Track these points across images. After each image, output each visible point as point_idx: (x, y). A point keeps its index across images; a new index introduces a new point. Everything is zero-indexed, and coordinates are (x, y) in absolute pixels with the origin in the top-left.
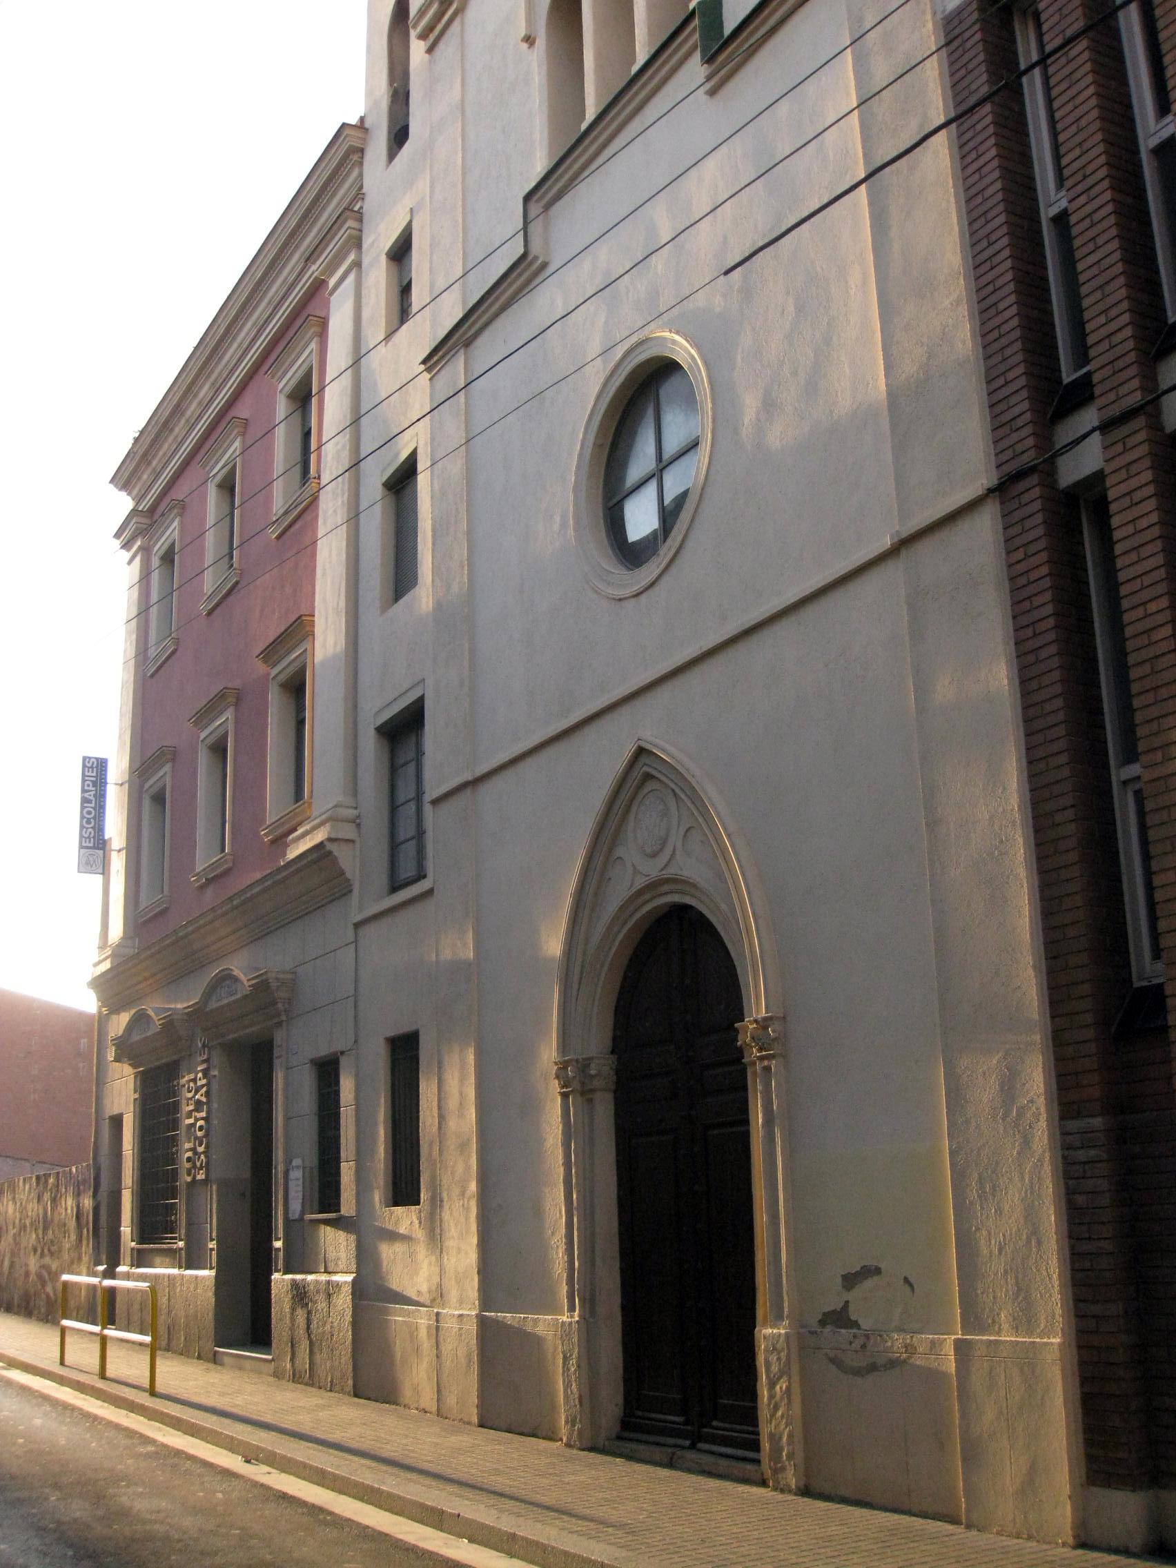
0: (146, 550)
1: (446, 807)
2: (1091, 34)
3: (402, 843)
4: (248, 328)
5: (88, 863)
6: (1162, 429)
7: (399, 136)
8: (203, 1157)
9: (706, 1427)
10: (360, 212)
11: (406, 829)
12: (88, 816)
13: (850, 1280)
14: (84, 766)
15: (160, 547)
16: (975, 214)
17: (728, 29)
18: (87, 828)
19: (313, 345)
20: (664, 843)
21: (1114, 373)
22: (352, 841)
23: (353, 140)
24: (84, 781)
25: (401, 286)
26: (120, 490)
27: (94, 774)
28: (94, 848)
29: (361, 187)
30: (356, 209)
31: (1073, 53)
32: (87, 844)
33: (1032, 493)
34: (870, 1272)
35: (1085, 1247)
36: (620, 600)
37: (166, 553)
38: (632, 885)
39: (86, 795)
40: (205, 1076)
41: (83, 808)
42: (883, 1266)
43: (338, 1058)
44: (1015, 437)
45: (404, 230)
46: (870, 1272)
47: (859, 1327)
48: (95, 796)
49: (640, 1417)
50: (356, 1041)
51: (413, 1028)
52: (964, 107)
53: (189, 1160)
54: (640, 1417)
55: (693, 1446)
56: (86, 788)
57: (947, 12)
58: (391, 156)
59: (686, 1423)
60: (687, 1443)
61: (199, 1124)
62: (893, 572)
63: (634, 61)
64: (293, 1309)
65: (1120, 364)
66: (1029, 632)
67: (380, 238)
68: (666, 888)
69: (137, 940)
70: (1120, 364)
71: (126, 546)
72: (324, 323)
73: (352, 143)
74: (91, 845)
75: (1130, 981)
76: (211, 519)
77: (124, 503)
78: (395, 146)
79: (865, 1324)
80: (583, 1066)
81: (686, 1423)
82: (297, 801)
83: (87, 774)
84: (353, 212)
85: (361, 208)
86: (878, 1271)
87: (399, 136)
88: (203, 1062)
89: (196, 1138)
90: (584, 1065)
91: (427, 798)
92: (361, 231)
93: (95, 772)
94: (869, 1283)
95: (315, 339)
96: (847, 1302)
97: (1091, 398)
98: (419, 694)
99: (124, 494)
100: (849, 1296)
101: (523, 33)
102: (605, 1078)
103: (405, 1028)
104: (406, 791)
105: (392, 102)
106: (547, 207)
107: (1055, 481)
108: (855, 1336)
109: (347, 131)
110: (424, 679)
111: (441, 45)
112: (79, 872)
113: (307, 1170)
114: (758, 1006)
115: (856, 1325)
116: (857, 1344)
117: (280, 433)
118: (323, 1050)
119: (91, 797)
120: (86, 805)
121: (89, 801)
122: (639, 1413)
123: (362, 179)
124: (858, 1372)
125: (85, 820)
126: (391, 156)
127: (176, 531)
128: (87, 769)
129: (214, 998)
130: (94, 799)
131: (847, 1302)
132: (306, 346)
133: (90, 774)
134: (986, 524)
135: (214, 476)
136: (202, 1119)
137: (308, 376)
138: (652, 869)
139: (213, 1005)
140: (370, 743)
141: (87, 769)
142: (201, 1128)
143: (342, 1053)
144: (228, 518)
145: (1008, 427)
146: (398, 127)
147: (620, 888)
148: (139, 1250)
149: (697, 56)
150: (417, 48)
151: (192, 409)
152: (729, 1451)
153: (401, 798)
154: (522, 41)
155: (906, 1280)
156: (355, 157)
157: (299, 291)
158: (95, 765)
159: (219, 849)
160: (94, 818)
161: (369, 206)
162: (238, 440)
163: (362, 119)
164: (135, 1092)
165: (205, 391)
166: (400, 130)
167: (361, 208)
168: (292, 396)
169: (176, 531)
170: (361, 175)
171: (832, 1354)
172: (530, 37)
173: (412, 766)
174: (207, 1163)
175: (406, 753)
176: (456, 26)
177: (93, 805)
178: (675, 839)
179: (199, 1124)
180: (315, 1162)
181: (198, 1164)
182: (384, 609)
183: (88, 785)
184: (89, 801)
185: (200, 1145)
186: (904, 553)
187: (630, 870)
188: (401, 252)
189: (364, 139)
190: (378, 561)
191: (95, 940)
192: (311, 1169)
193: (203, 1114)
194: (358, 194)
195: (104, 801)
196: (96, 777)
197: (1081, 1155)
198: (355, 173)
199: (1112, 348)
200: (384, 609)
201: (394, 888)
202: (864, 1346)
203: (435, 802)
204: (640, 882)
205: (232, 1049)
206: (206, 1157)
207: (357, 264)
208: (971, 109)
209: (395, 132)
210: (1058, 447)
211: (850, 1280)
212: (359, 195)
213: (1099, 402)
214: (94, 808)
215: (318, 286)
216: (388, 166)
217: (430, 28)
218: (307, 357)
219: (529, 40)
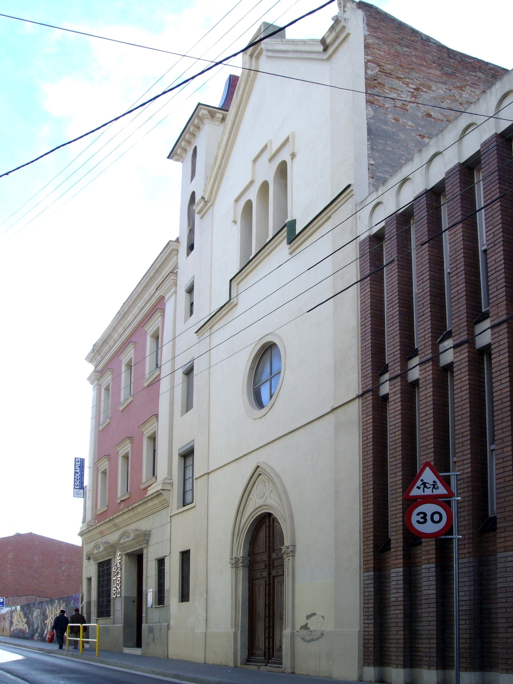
0: (100, 386)
1: (199, 480)
2: (502, 199)
3: (187, 491)
4: (136, 310)
5: (77, 494)
6: (407, 381)
7: (191, 247)
8: (119, 589)
9: (270, 660)
10: (176, 273)
11: (188, 487)
12: (78, 478)
13: (308, 617)
14: (75, 461)
15: (104, 384)
16: (363, 309)
17: (297, 233)
18: (77, 482)
19: (160, 319)
20: (264, 495)
21: (425, 355)
22: (170, 490)
23: (174, 246)
24: (75, 466)
25: (191, 302)
26: (89, 362)
27: (79, 464)
28: (79, 489)
29: (177, 264)
30: (175, 272)
31: (494, 207)
32: (77, 487)
33: (369, 397)
34: (314, 614)
35: (366, 606)
36: (255, 419)
37: (106, 387)
38: (254, 507)
39: (76, 471)
40: (120, 564)
41: (75, 475)
42: (316, 613)
43: (164, 558)
44: (367, 380)
45: (190, 285)
46: (314, 614)
47: (310, 629)
48: (80, 471)
49: (252, 658)
50: (170, 553)
51: (188, 549)
52: (452, 223)
53: (114, 590)
54: (252, 658)
55: (266, 665)
56: (76, 468)
57: (361, 240)
58: (188, 254)
59: (265, 659)
60: (264, 664)
61: (118, 579)
62: (331, 416)
63: (251, 255)
64: (149, 634)
65: (396, 361)
66: (366, 438)
67: (183, 284)
68: (264, 508)
69: (96, 520)
70: (396, 361)
71: (92, 383)
72: (163, 310)
73: (174, 248)
74: (79, 488)
75: (388, 537)
76: (148, 353)
77: (90, 368)
78: (190, 251)
79: (312, 629)
80: (237, 560)
81: (265, 659)
82: (153, 476)
83: (76, 463)
84: (174, 272)
85: (177, 272)
86: (315, 614)
87: (191, 247)
88: (120, 559)
89: (117, 584)
90: (237, 560)
91: (194, 478)
92: (177, 280)
93: (80, 464)
94: (313, 617)
95: (133, 349)
96: (307, 623)
97: (387, 371)
98: (193, 444)
99: (90, 364)
100: (308, 621)
101: (232, 219)
102: (245, 563)
103: (186, 549)
104: (189, 474)
105: (189, 233)
106: (238, 284)
107: (379, 394)
108: (308, 632)
109: (171, 243)
110: (194, 440)
111: (206, 216)
112: (74, 497)
113: (154, 592)
114: (287, 543)
115: (309, 629)
116: (309, 634)
117: (123, 375)
118: (160, 556)
119: (78, 471)
120: (76, 474)
121: (78, 473)
122: (252, 657)
123: (178, 261)
124: (309, 641)
125: (76, 479)
126: (188, 254)
127: (133, 354)
128: (76, 462)
129: (122, 539)
130: (79, 472)
131: (307, 623)
132: (130, 351)
133: (78, 463)
134: (356, 405)
135: (103, 385)
136: (119, 577)
137: (158, 329)
138: (260, 502)
139: (122, 541)
140: (176, 458)
141: (76, 462)
142: (119, 580)
143: (166, 556)
144: (155, 353)
145: (365, 377)
146: (190, 244)
147: (250, 508)
148: (97, 620)
149: (286, 240)
150: (197, 217)
151: (116, 336)
152: (276, 665)
153: (187, 477)
154: (232, 222)
155: (322, 616)
156: (175, 252)
157: (142, 315)
158: (80, 461)
159: (126, 491)
160: (80, 479)
161: (180, 271)
162: (160, 317)
163: (178, 239)
164: (95, 569)
165: (120, 330)
166: (191, 245)
167: (177, 272)
168: (152, 336)
169: (133, 354)
170: (177, 259)
171: (302, 637)
172: (235, 221)
173: (191, 467)
174: (121, 592)
175: (189, 462)
176: (210, 210)
177: (79, 474)
178: (267, 493)
179: (118, 579)
180: (157, 590)
181: (118, 592)
182: (182, 415)
183: (77, 467)
184: (78, 473)
185: (118, 586)
186: (335, 411)
187: (254, 502)
188: (190, 290)
189: (178, 246)
190: (180, 398)
191: (81, 520)
192: (155, 592)
193: (120, 576)
194: (176, 267)
195: (84, 473)
196: (80, 465)
197: (367, 582)
198: (175, 258)
199: (394, 356)
200: (182, 415)
201: (184, 506)
202: (310, 634)
203: (196, 479)
204: (257, 506)
205: (129, 555)
206: (120, 589)
207: (175, 292)
208: (454, 225)
209: (189, 245)
210: (381, 383)
211: (308, 617)
212: (176, 267)
213: (389, 372)
214: (80, 475)
215: (162, 298)
216: (187, 258)
217: (201, 210)
218: (158, 323)
219: (235, 222)
